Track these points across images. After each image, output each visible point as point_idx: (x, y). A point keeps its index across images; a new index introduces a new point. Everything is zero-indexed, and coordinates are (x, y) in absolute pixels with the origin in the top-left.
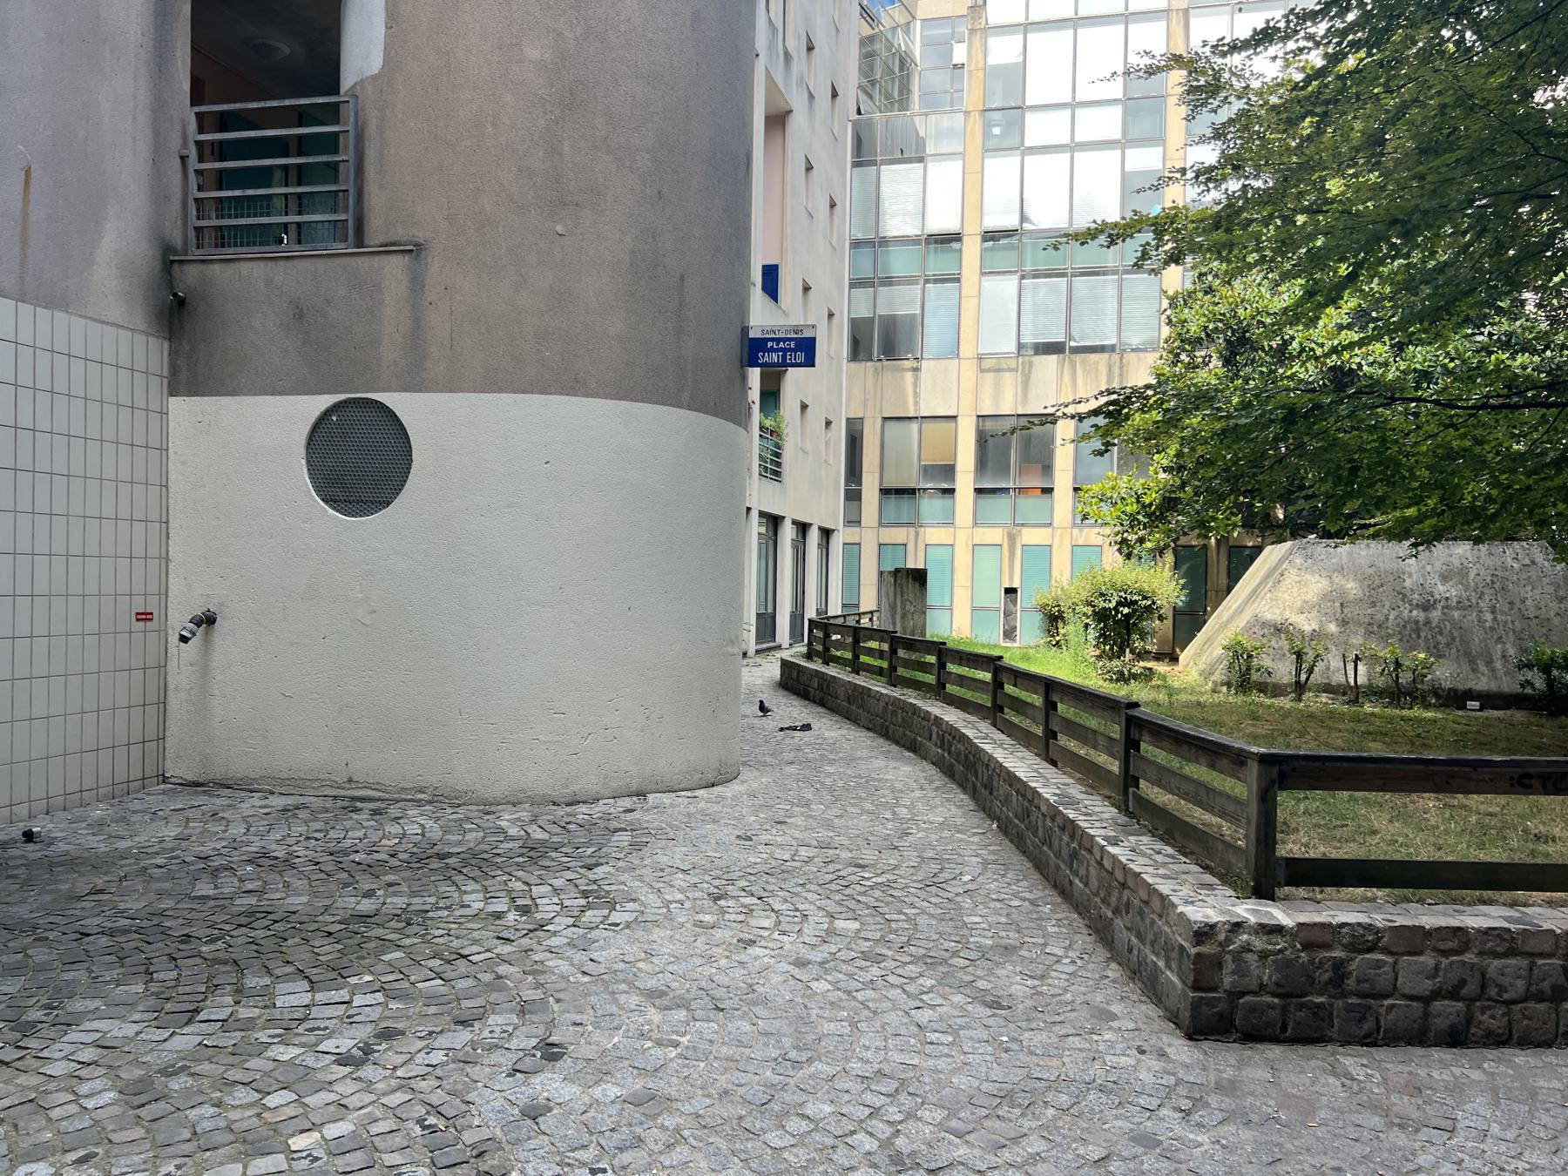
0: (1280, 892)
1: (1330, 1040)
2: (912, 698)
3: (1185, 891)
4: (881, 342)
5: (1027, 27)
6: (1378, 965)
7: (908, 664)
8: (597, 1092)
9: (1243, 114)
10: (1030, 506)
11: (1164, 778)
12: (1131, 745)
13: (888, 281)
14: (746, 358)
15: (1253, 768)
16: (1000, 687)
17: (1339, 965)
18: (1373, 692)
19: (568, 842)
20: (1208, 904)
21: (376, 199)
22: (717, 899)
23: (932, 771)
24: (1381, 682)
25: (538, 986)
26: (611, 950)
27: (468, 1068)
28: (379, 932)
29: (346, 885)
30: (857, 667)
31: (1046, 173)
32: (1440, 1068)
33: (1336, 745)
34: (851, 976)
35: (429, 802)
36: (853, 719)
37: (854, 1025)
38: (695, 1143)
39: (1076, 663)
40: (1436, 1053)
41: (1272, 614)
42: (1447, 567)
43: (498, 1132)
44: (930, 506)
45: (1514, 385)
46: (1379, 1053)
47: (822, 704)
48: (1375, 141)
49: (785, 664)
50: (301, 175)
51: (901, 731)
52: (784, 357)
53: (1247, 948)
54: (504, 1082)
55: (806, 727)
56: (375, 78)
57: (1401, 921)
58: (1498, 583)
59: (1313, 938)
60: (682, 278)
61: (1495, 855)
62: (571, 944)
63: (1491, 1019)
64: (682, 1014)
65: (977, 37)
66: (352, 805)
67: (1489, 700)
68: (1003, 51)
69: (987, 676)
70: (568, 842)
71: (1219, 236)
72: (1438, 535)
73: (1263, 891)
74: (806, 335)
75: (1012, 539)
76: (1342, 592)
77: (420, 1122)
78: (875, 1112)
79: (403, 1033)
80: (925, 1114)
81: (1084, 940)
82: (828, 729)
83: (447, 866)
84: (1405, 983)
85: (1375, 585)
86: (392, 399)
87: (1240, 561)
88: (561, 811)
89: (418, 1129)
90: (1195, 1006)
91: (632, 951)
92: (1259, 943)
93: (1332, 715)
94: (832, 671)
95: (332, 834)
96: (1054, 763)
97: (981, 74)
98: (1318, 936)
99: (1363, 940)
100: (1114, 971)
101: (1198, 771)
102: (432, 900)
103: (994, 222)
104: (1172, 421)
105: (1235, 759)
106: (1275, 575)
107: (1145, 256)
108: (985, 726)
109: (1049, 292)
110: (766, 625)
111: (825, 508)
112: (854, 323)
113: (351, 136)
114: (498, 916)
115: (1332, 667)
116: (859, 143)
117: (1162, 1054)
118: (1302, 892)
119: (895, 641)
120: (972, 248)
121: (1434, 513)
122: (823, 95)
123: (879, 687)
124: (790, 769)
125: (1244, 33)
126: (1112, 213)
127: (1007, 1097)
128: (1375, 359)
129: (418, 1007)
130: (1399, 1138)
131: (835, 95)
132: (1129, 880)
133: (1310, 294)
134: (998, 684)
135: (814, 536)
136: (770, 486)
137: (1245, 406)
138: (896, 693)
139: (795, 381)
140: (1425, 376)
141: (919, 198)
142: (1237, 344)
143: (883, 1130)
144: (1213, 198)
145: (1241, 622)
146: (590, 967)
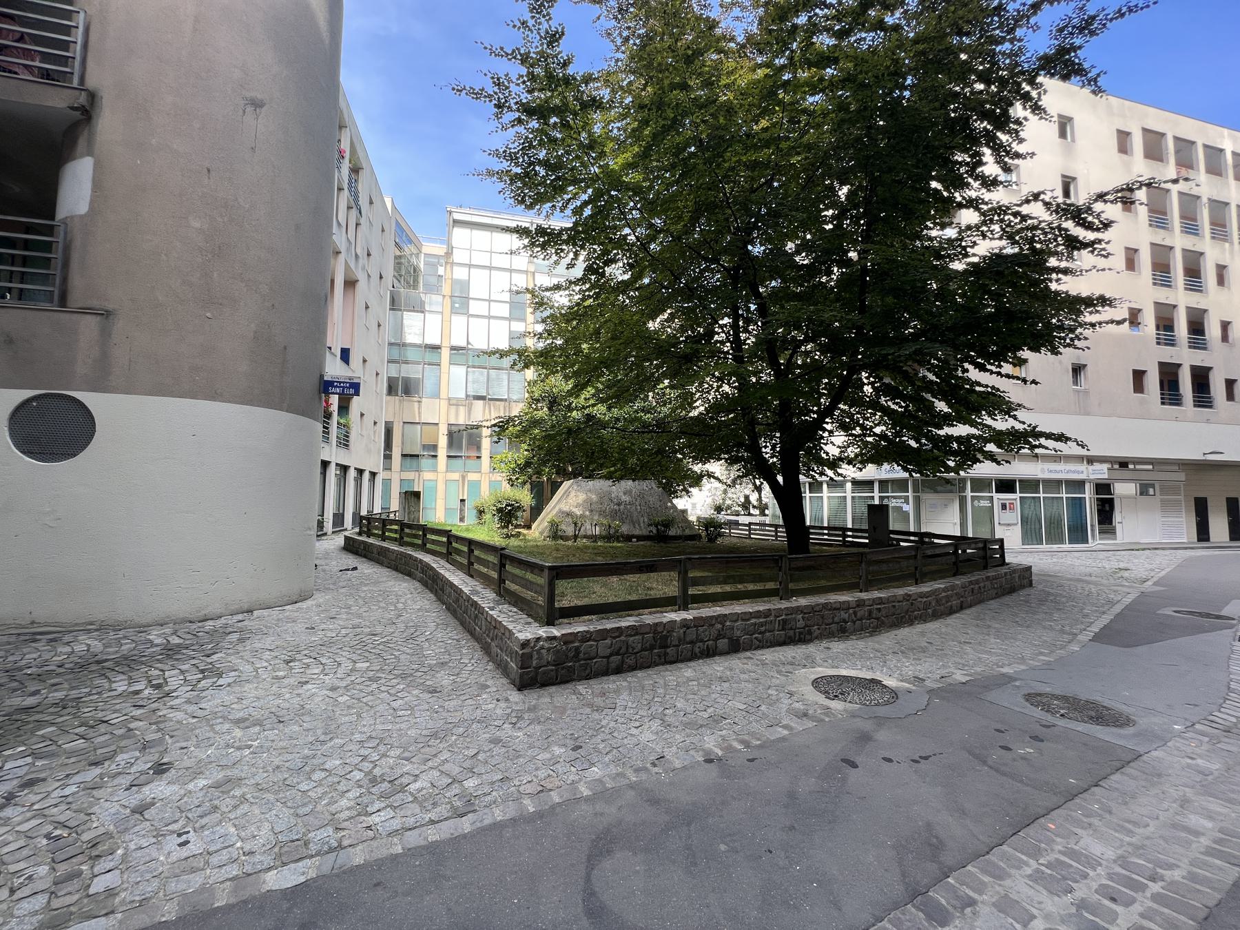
0: (557, 622)
1: (572, 680)
2: (410, 551)
3: (519, 627)
4: (401, 388)
6: (591, 646)
7: (408, 535)
8: (191, 786)
9: (552, 315)
10: (471, 463)
11: (515, 579)
12: (502, 566)
13: (406, 362)
15: (546, 571)
16: (454, 546)
17: (577, 648)
18: (602, 537)
19: (197, 643)
20: (526, 630)
21: (77, 282)
22: (288, 662)
23: (418, 584)
24: (604, 533)
25: (159, 730)
26: (213, 701)
27: (95, 792)
28: (37, 717)
29: (15, 690)
30: (384, 538)
31: (478, 326)
32: (611, 683)
33: (585, 559)
34: (361, 691)
35: (96, 630)
36: (380, 563)
37: (359, 716)
38: (252, 800)
39: (488, 533)
40: (612, 678)
41: (566, 509)
42: (624, 490)
43: (112, 827)
44: (425, 462)
45: (645, 425)
46: (591, 682)
47: (365, 557)
48: (597, 332)
49: (346, 538)
50: (25, 261)
51: (403, 567)
53: (542, 648)
54: (122, 794)
55: (355, 569)
56: (81, 216)
57: (599, 628)
58: (641, 495)
59: (567, 639)
60: (285, 348)
61: (634, 597)
62: (188, 702)
63: (630, 661)
64: (257, 729)
66: (33, 638)
67: (640, 538)
68: (460, 273)
69: (445, 539)
70: (197, 643)
71: (544, 359)
72: (621, 478)
73: (550, 623)
75: (463, 478)
76: (591, 499)
77: (48, 836)
78: (365, 758)
79: (44, 780)
80: (392, 753)
81: (479, 654)
82: (367, 569)
83: (103, 668)
84: (601, 653)
85: (603, 497)
86: (90, 399)
87: (555, 487)
88: (194, 626)
89: (45, 842)
90: (521, 676)
91: (228, 699)
92: (547, 645)
93: (586, 547)
94: (371, 540)
95: (11, 658)
96: (472, 576)
98: (572, 638)
99: (586, 637)
100: (491, 666)
101: (529, 576)
102: (87, 690)
103: (455, 343)
104: (525, 431)
105: (541, 568)
106: (567, 493)
107: (515, 364)
108: (443, 562)
109: (479, 375)
110: (339, 519)
111: (373, 462)
112: (390, 380)
113: (61, 245)
114: (137, 692)
115: (588, 529)
116: (393, 301)
117: (507, 700)
118: (566, 621)
119: (403, 525)
120: (445, 354)
121: (619, 470)
122: (375, 277)
123: (394, 547)
124: (343, 590)
125: (550, 285)
126: (504, 345)
127: (434, 735)
128: (600, 410)
129: (63, 760)
130: (596, 716)
131: (381, 277)
132: (496, 625)
133: (575, 386)
134: (449, 543)
135: (366, 476)
136: (342, 451)
137: (553, 426)
138: (402, 549)
139: (356, 404)
140: (618, 420)
141: (415, 329)
142: (553, 402)
143: (367, 766)
144: (541, 345)
145: (554, 512)
146: (200, 713)
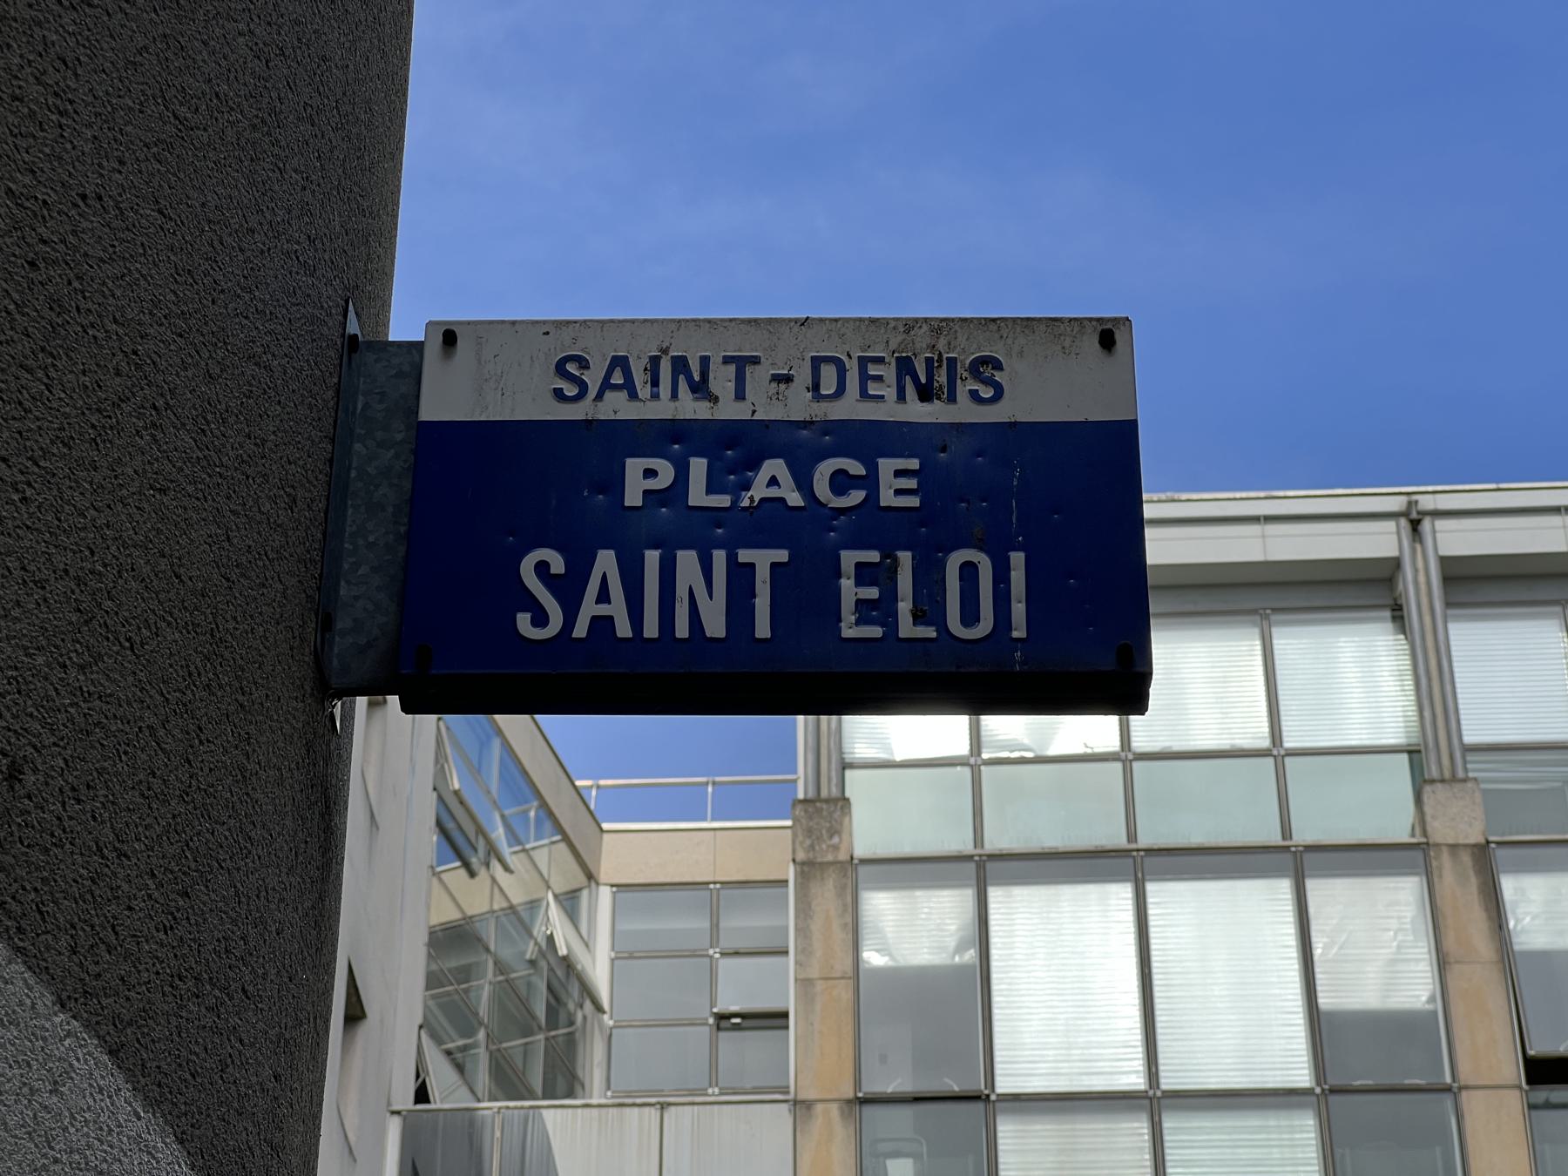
5: (983, 869)
14: (367, 601)
52: (804, 592)
65: (826, 894)
68: (909, 930)
74: (1039, 395)
97: (844, 993)
